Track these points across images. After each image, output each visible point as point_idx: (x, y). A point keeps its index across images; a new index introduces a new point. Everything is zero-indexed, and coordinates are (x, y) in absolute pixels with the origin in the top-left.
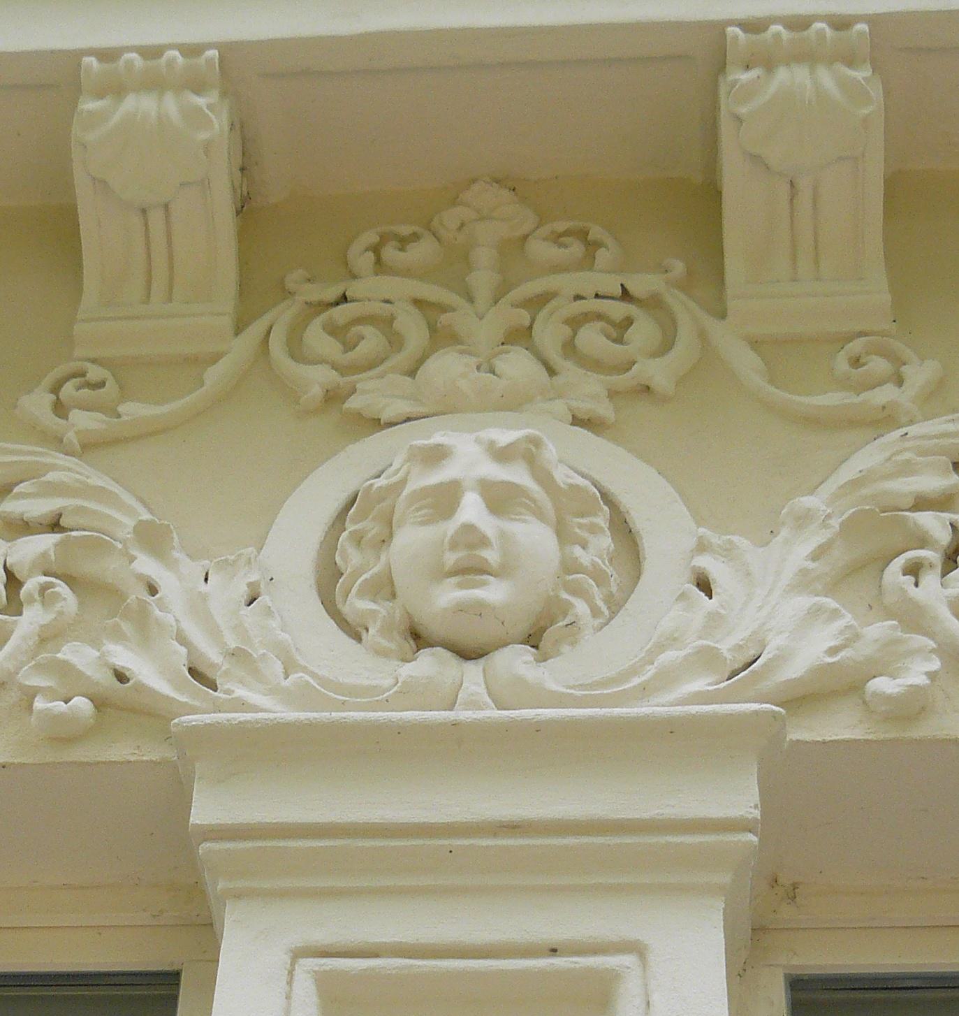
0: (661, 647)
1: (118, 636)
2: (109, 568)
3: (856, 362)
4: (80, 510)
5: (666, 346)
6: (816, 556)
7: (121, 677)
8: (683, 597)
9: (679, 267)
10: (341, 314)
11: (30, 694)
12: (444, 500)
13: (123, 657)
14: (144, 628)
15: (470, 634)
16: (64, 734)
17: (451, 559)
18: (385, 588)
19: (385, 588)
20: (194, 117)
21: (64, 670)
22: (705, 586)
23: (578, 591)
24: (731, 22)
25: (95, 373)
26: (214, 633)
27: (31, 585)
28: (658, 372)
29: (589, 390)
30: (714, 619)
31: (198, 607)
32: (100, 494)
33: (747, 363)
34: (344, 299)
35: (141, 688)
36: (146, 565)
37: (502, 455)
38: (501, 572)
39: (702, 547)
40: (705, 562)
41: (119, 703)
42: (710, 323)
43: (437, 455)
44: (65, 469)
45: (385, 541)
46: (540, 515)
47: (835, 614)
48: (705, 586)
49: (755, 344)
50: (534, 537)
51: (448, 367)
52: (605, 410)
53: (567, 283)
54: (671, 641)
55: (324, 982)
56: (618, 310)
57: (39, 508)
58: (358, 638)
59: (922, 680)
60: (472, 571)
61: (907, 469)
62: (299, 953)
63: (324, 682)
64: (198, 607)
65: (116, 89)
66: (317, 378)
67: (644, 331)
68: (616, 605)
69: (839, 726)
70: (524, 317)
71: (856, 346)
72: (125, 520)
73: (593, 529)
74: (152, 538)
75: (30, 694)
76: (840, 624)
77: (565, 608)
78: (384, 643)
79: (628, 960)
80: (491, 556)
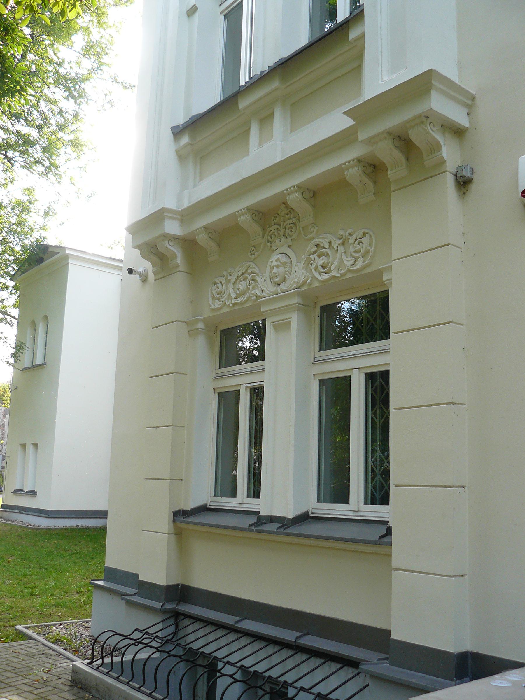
61: (312, 248)
69: (305, 288)
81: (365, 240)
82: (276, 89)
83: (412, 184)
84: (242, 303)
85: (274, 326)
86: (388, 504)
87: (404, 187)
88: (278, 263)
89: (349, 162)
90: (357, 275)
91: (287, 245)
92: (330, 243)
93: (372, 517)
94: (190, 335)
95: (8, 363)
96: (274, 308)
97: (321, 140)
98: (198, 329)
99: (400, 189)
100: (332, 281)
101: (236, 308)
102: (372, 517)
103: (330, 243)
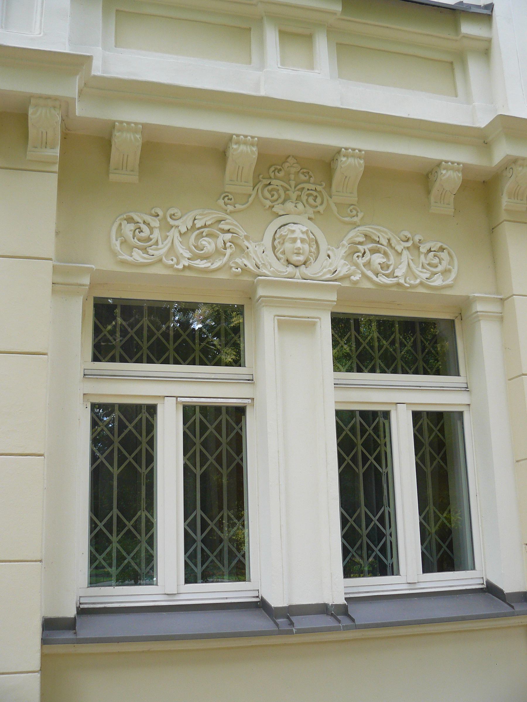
0: (323, 269)
1: (244, 257)
2: (239, 242)
3: (351, 211)
4: (233, 229)
5: (322, 203)
6: (344, 253)
7: (246, 266)
8: (327, 259)
9: (324, 184)
10: (270, 187)
11: (231, 267)
12: (294, 240)
13: (246, 262)
14: (248, 256)
15: (297, 264)
16: (237, 275)
17: (296, 251)
18: (283, 253)
19: (283, 253)
20: (252, 151)
21: (236, 263)
22: (329, 256)
23: (311, 256)
24: (343, 148)
25: (230, 197)
26: (258, 258)
27: (228, 244)
28: (321, 209)
29: (311, 211)
30: (331, 264)
31: (255, 252)
32: (236, 226)
33: (334, 209)
34: (270, 184)
35: (249, 268)
36: (246, 243)
37: (303, 233)
38: (303, 254)
39: (329, 249)
40: (329, 252)
41: (245, 270)
42: (329, 198)
43: (293, 232)
44: (230, 219)
45: (283, 243)
46: (307, 243)
47: (347, 265)
48: (329, 256)
49: (336, 204)
50: (306, 247)
51: (290, 205)
52: (312, 216)
53: (307, 186)
54: (325, 267)
55: (278, 320)
56: (315, 193)
57: (226, 227)
58: (279, 260)
59: (358, 278)
60: (298, 254)
61: (358, 236)
62: (275, 316)
63: (276, 270)
64: (255, 252)
65: (238, 143)
66: (268, 203)
67: (319, 200)
68: (316, 258)
69: (346, 284)
70: (299, 193)
71: (352, 207)
72: (242, 233)
73: (314, 244)
74: (247, 238)
75: (231, 267)
76: (348, 267)
77: (310, 259)
78: (284, 263)
79: (318, 320)
80: (301, 251)
81: (444, 255)
82: (334, 14)
83: (11, 169)
84: (205, 271)
85: (279, 321)
86: (424, 571)
87: (520, 222)
88: (305, 237)
89: (453, 163)
90: (432, 292)
91: (307, 216)
92: (389, 240)
93: (455, 586)
94: (54, 292)
95: (284, 265)
96: (306, 297)
97: (410, 117)
98: (81, 285)
99: (514, 222)
100: (394, 289)
101: (188, 273)
102: (435, 587)
103: (389, 240)
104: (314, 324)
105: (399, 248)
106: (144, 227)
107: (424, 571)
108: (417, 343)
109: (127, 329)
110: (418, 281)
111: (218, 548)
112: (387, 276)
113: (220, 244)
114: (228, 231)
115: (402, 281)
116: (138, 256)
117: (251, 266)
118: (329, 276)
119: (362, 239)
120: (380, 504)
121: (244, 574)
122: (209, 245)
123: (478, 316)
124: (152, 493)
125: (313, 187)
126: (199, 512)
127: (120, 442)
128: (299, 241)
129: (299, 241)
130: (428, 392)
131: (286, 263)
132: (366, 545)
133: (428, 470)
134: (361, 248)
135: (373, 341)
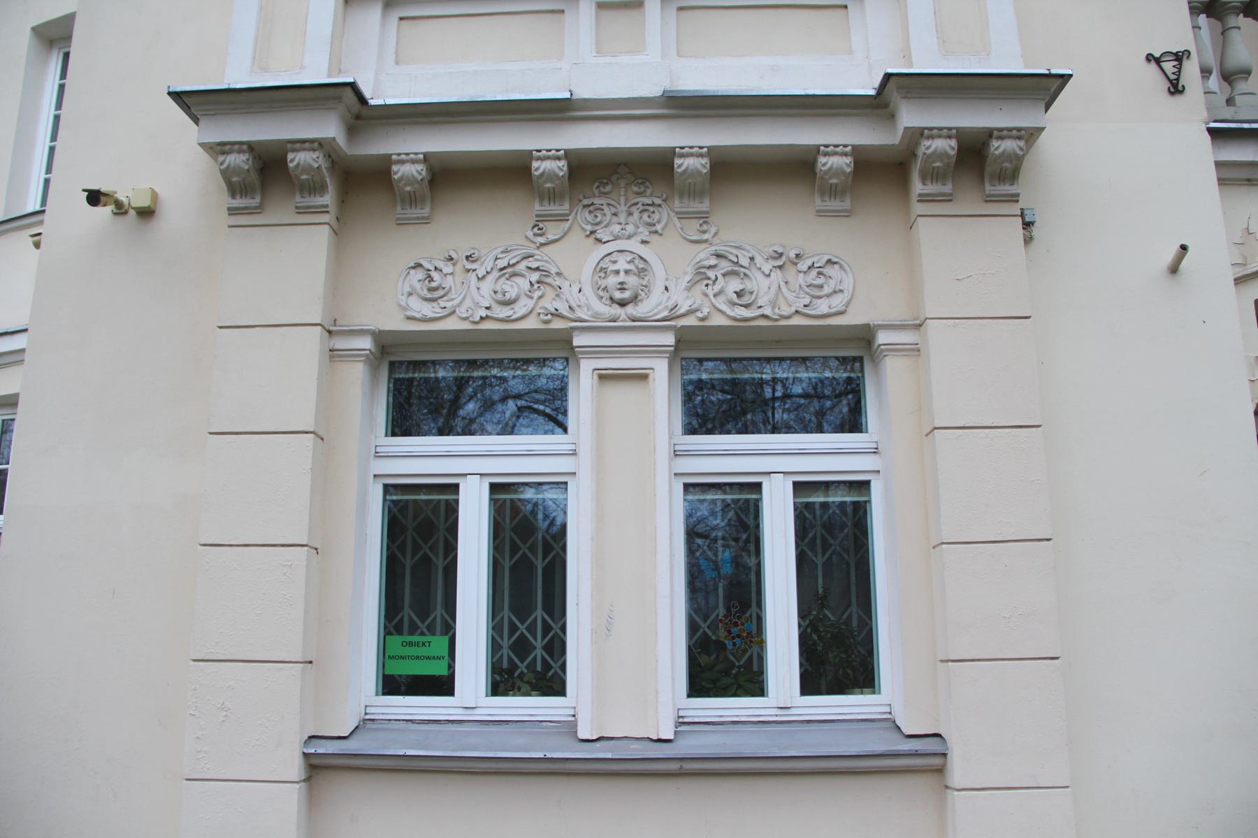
12: (617, 272)
41: (557, 315)
48: (666, 289)
57: (534, 265)
60: (622, 289)
61: (707, 259)
66: (589, 228)
86: (689, 696)
104: (644, 377)
105: (766, 269)
106: (435, 275)
107: (689, 696)
108: (825, 382)
109: (427, 387)
110: (793, 310)
111: (532, 659)
112: (746, 306)
113: (527, 286)
114: (537, 269)
115: (768, 311)
116: (428, 310)
117: (564, 310)
118: (665, 313)
119: (713, 261)
120: (745, 606)
121: (873, 686)
122: (512, 288)
123: (882, 351)
124: (462, 587)
125: (648, 201)
126: (506, 612)
127: (417, 529)
128: (622, 273)
129: (622, 273)
130: (824, 454)
131: (608, 302)
132: (722, 658)
133: (439, 611)
134: (711, 274)
135: (729, 389)
